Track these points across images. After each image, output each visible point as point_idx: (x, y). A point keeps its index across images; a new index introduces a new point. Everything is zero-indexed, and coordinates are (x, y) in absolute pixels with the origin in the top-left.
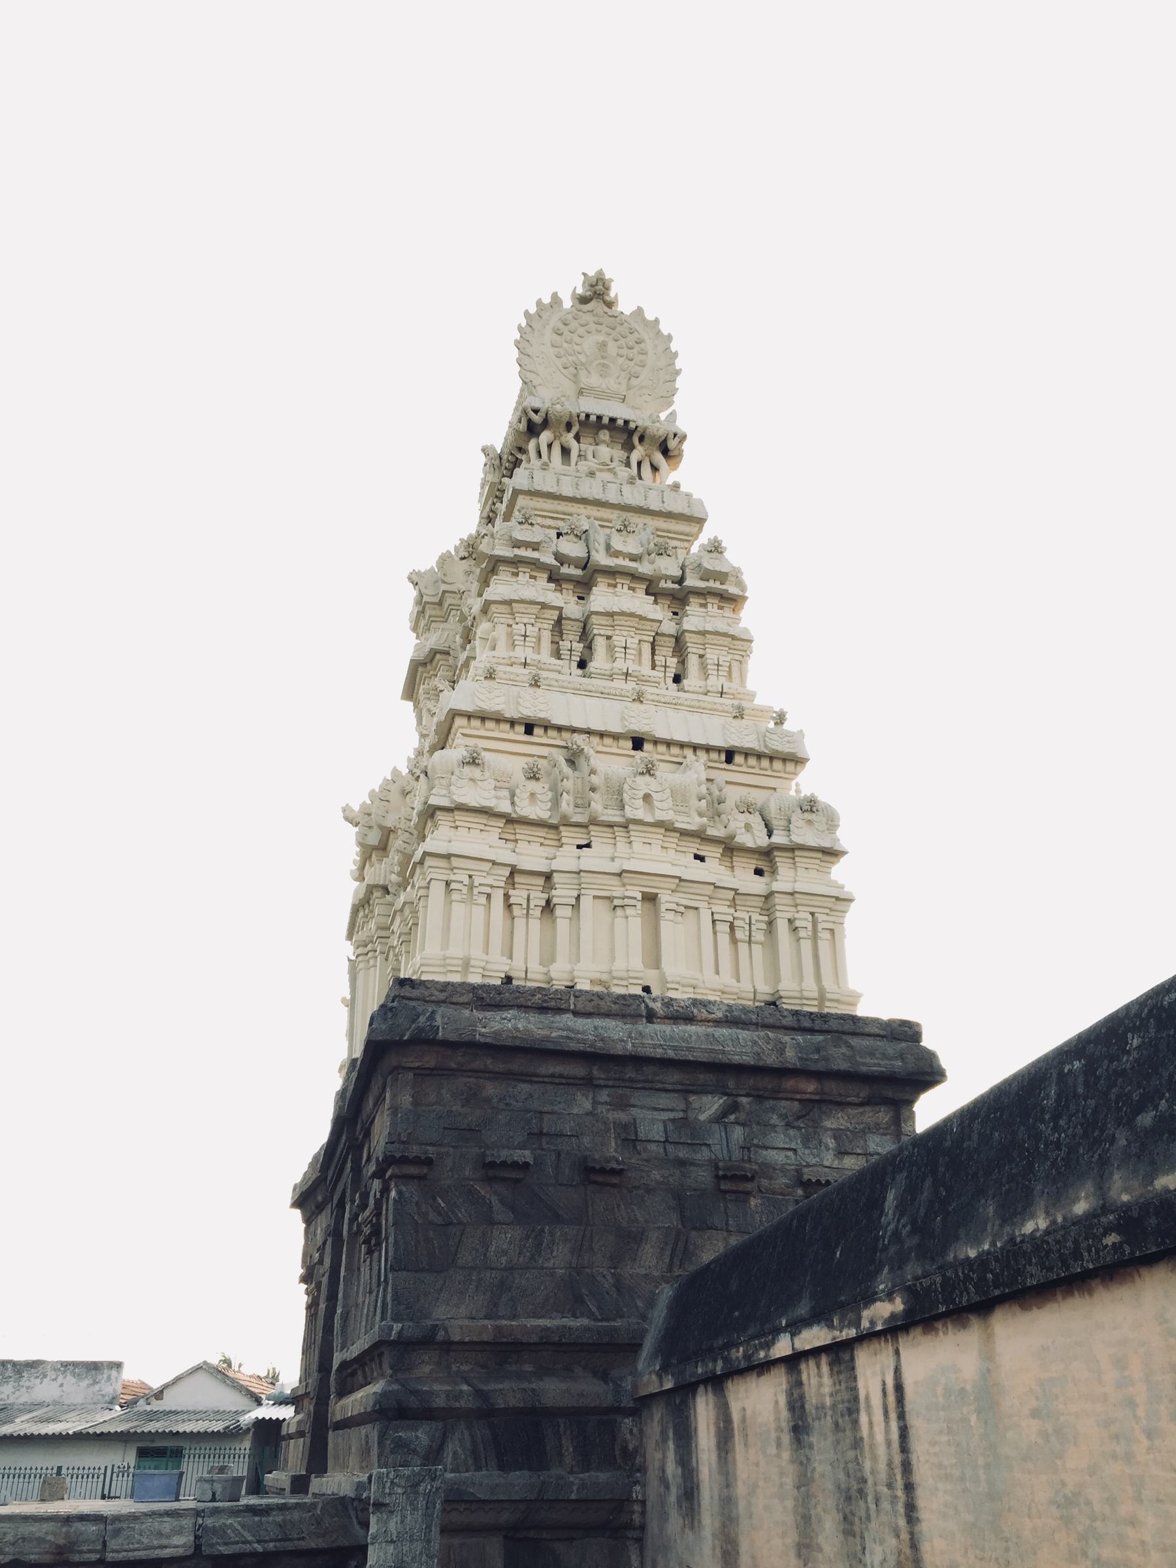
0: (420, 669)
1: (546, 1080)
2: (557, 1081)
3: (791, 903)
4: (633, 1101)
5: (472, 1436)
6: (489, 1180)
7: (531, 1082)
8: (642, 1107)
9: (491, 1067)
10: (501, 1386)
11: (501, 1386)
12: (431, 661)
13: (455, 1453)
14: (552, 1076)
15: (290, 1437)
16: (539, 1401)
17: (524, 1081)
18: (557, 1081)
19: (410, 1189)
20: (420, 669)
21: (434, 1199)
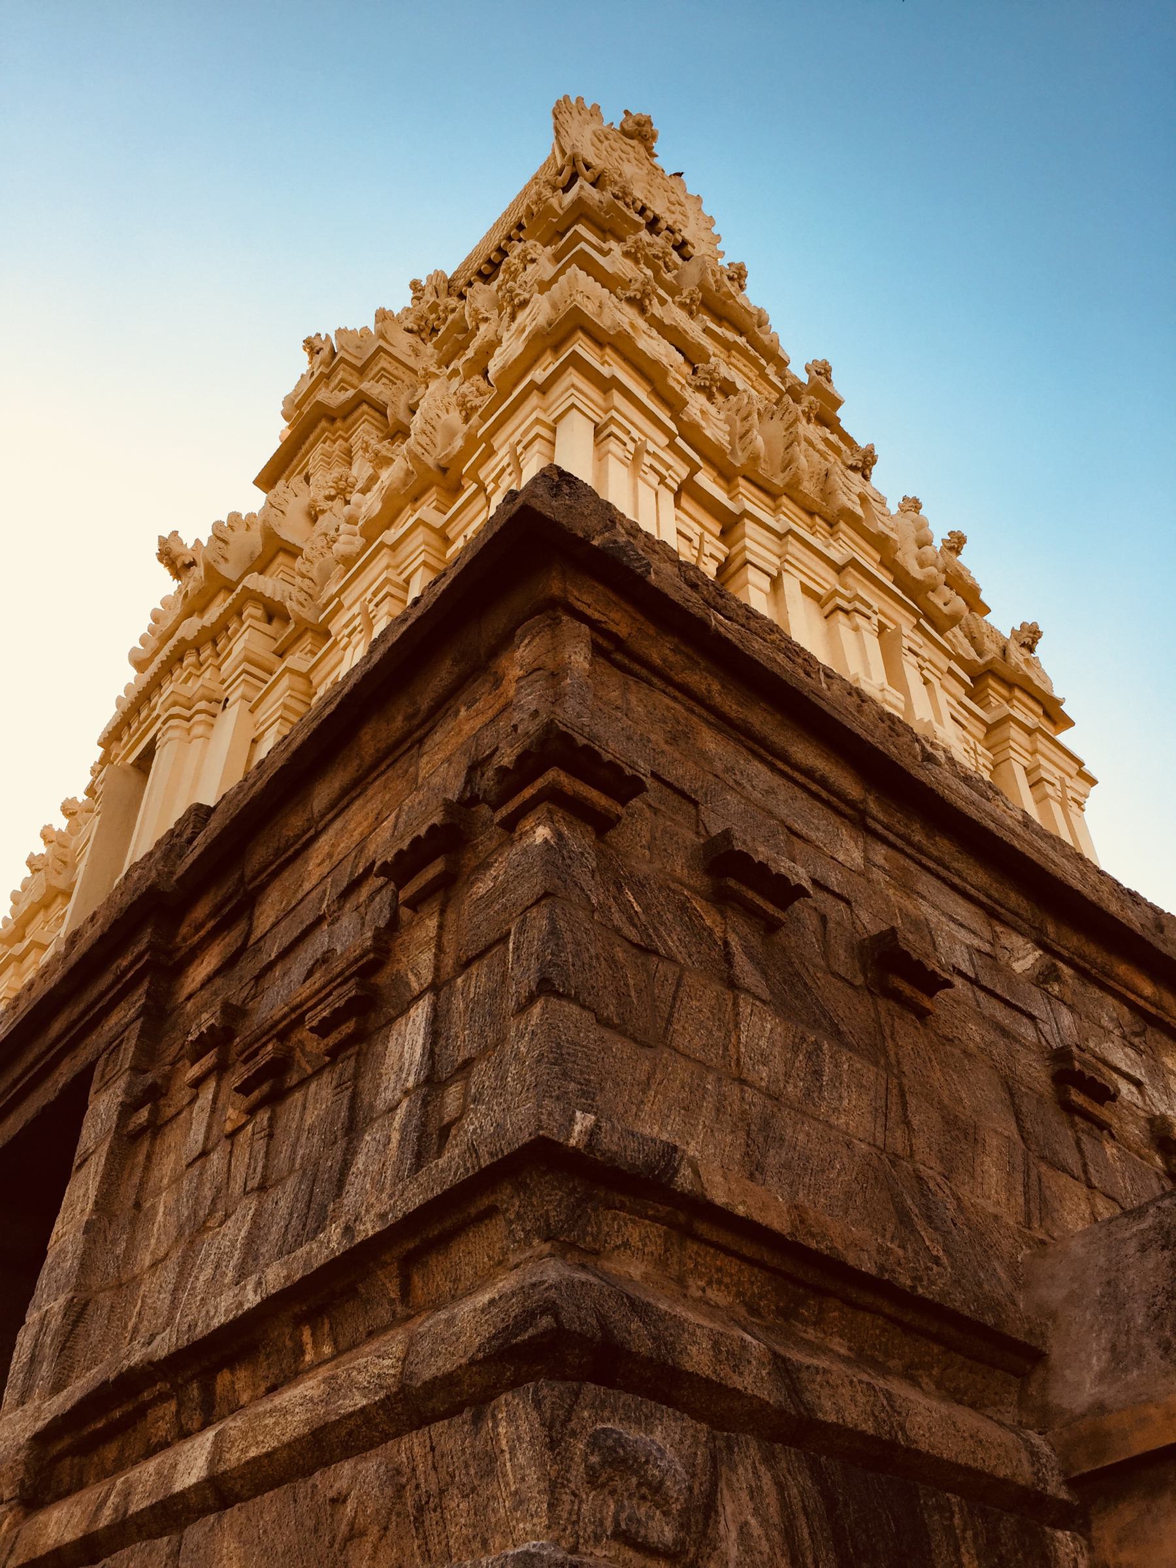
0: (324, 424)
1: (796, 775)
2: (814, 787)
3: (1028, 747)
4: (920, 887)
5: (781, 1487)
6: (721, 899)
7: (773, 768)
8: (935, 906)
9: (718, 699)
10: (815, 1362)
11: (815, 1362)
12: (345, 418)
13: (743, 1528)
14: (809, 773)
15: (1161, 998)
16: (902, 1427)
17: (763, 760)
18: (814, 787)
19: (579, 840)
20: (324, 424)
21: (620, 889)
